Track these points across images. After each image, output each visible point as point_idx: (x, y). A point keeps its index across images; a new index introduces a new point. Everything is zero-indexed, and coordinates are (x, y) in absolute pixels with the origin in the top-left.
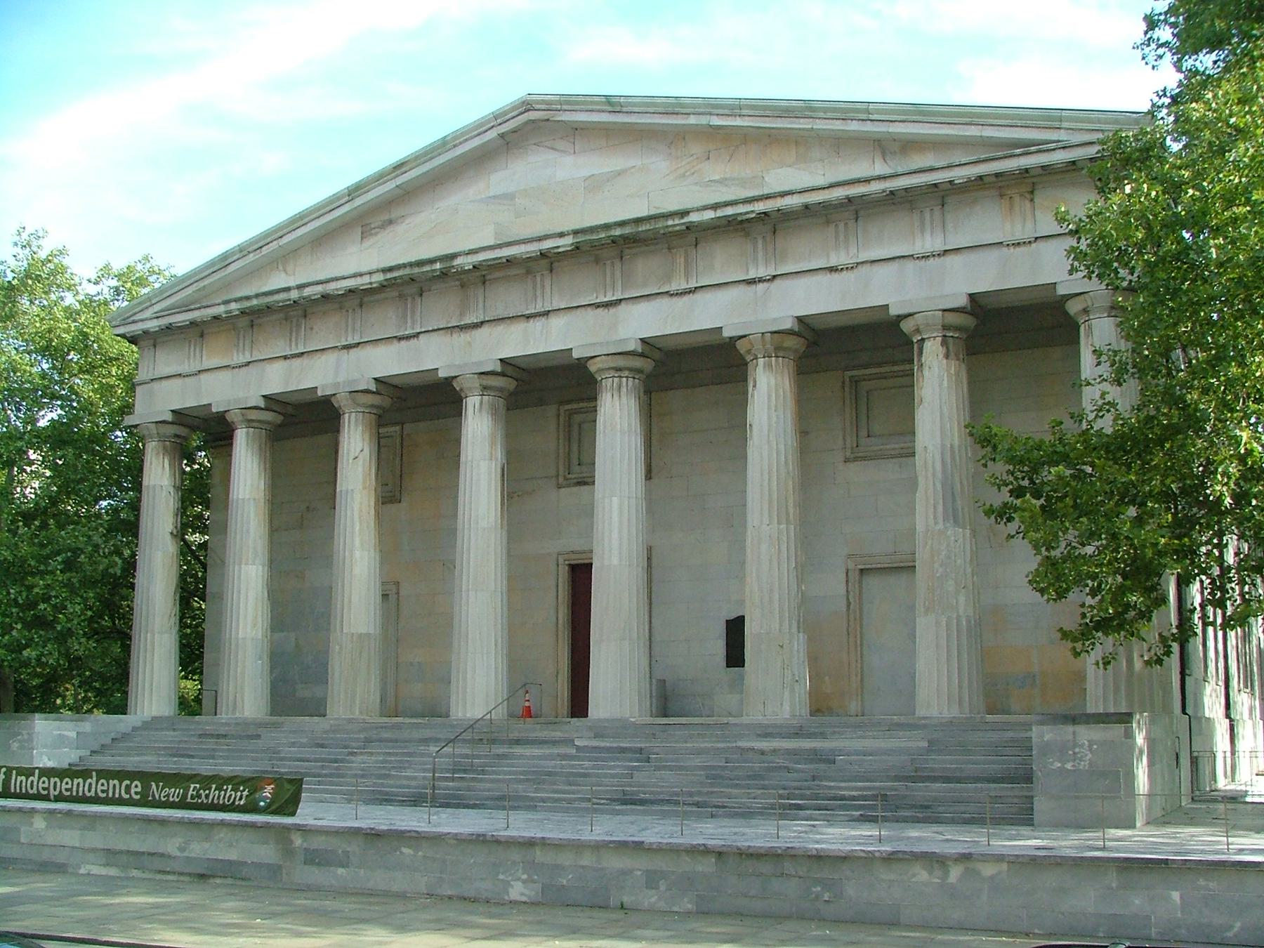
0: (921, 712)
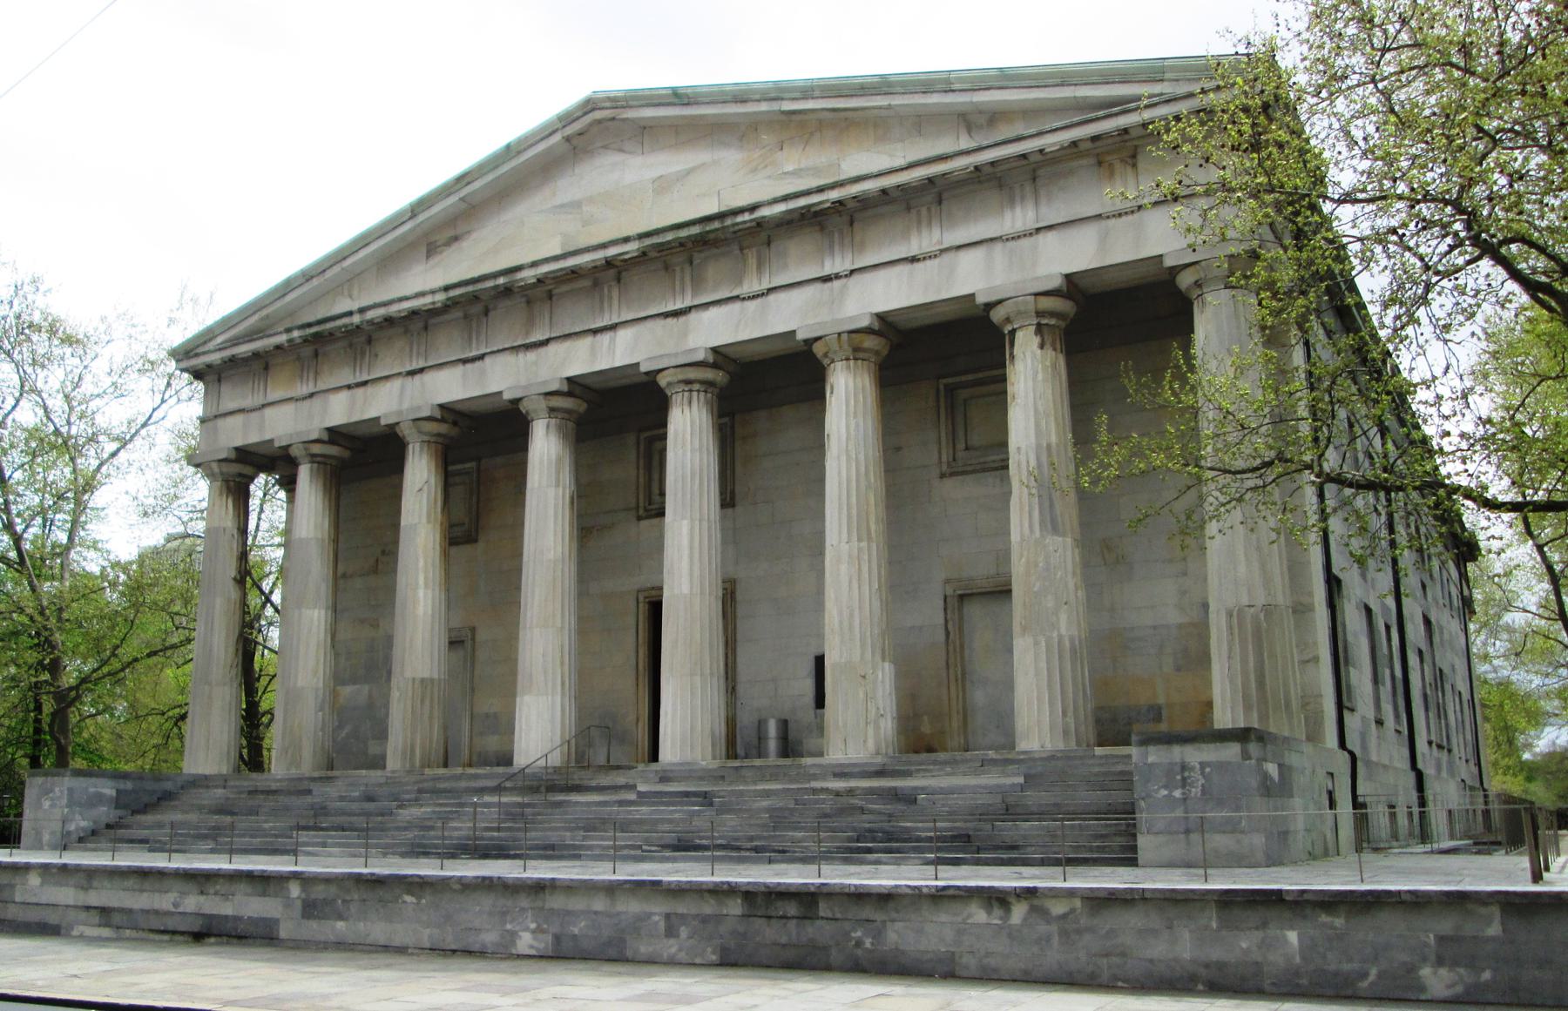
0: (1022, 745)
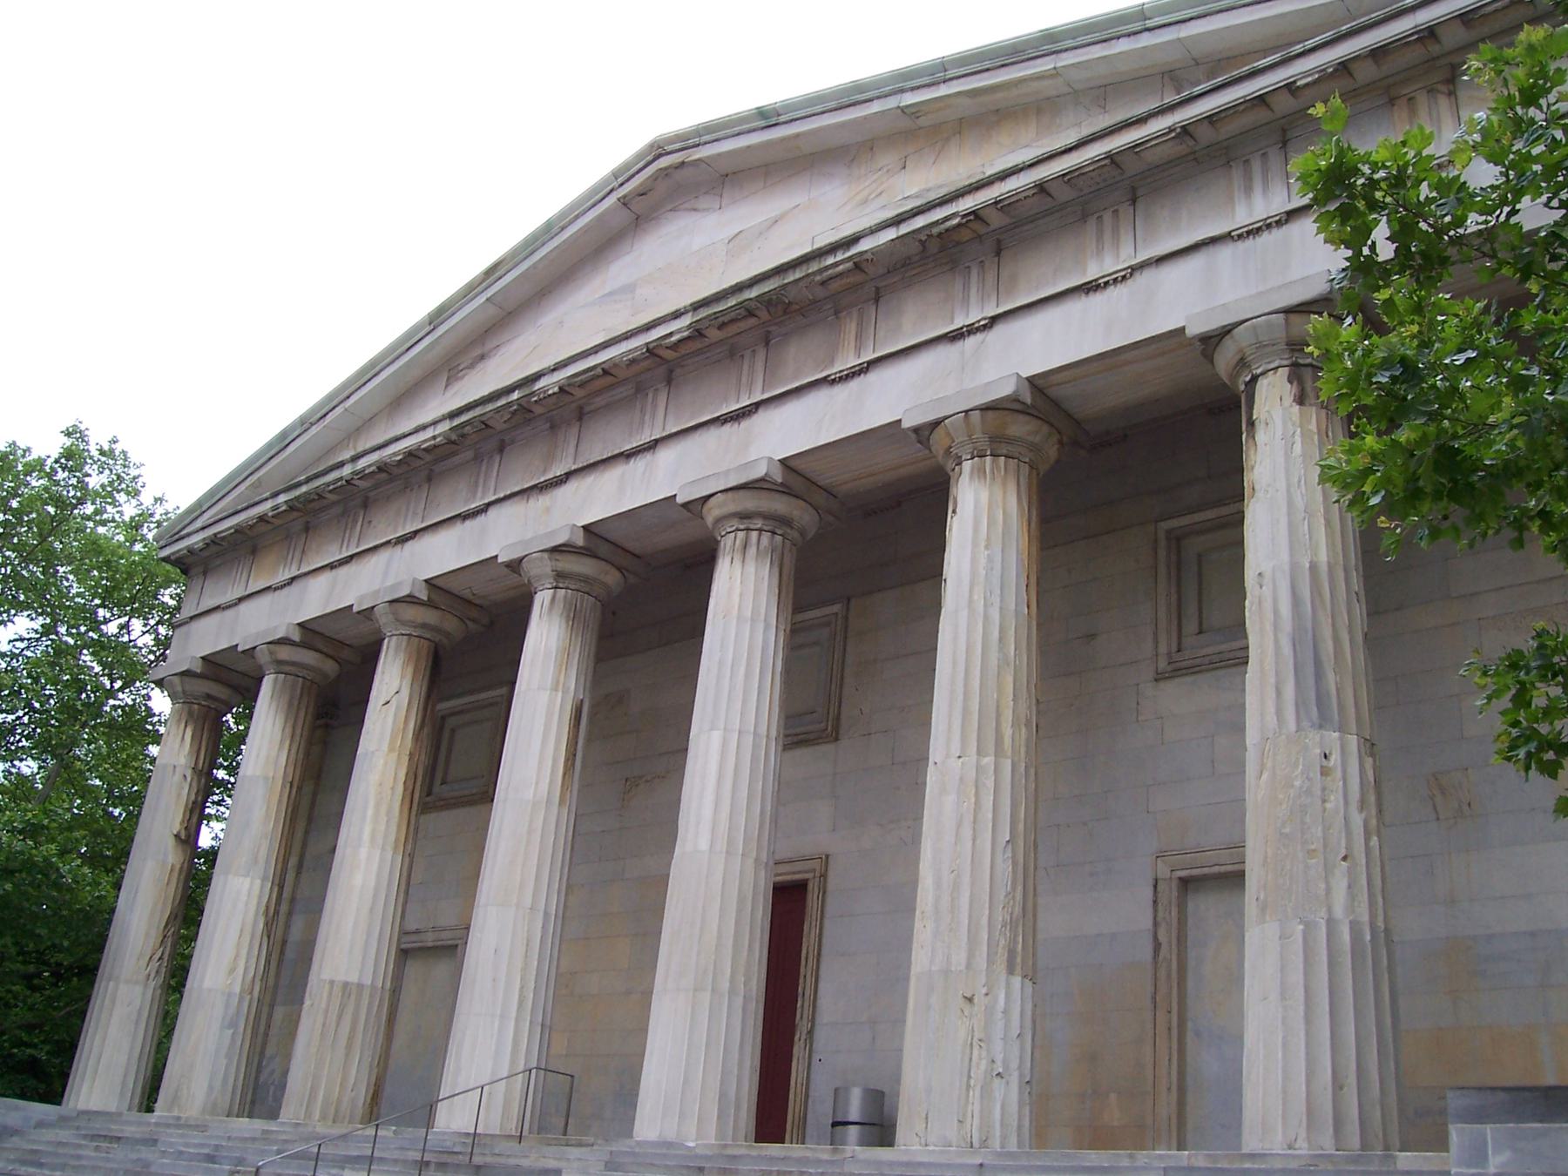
0: (1250, 1143)
